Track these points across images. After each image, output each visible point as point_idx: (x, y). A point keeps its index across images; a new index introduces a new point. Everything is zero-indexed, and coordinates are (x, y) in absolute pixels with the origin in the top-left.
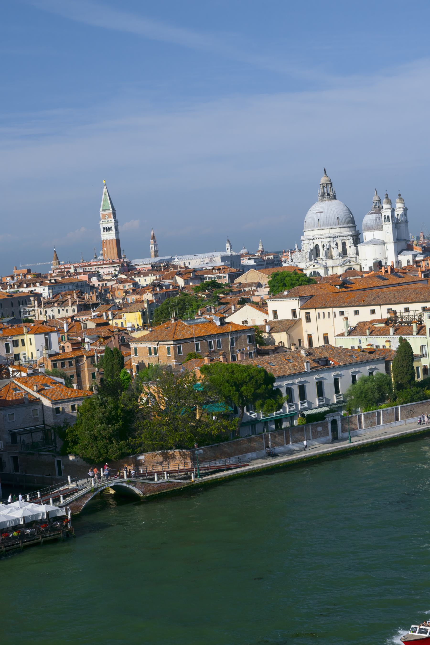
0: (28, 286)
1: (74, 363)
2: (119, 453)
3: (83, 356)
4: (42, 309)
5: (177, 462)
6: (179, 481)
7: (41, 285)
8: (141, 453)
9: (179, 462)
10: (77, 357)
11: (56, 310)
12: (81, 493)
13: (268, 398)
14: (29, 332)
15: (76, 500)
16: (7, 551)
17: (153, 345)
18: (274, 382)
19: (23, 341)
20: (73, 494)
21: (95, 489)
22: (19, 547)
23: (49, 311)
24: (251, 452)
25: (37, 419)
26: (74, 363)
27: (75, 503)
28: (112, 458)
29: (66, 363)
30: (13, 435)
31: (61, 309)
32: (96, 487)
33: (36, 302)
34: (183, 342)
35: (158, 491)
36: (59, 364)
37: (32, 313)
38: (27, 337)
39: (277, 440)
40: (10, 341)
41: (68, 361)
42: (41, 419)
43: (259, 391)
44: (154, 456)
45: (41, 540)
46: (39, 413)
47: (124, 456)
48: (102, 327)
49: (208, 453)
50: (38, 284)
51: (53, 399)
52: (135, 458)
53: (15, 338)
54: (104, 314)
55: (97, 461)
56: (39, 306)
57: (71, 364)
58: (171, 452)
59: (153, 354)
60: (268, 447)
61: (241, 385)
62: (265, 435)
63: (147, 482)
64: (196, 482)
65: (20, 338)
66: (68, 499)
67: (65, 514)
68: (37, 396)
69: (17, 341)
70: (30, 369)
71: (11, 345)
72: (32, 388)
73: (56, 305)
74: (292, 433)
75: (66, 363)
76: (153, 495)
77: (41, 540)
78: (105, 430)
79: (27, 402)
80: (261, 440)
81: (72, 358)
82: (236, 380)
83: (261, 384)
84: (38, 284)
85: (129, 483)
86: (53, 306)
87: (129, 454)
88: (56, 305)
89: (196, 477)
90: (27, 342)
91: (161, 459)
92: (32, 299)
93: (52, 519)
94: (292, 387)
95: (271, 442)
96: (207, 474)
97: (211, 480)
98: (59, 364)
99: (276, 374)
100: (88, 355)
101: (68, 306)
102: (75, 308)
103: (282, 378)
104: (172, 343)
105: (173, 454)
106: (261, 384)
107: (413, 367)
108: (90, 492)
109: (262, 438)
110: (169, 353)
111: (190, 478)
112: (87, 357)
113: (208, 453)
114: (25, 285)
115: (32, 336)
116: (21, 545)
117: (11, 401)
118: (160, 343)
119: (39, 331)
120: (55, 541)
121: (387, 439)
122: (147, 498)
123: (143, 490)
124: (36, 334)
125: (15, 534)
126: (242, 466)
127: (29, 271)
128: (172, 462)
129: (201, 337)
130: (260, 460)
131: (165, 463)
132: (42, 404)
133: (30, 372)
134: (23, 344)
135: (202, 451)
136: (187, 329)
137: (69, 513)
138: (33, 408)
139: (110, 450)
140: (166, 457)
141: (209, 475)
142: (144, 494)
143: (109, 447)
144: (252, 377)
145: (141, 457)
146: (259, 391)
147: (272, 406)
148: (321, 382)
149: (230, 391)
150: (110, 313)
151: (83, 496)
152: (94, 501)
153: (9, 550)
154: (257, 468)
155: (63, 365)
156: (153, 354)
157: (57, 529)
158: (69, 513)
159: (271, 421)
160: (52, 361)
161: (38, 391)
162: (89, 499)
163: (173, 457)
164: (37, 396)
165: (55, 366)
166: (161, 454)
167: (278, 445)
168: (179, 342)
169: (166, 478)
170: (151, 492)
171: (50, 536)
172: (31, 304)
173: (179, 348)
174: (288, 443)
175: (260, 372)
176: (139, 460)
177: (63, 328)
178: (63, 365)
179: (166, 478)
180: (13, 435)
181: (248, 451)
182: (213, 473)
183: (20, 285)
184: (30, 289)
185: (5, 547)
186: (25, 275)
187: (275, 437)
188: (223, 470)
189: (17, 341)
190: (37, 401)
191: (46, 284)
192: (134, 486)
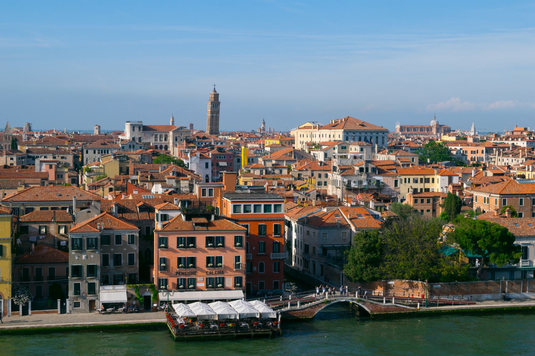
0: (512, 140)
1: (431, 201)
2: (371, 276)
3: (439, 197)
4: (501, 158)
5: (419, 291)
6: (405, 307)
7: (522, 140)
8: (391, 279)
9: (419, 291)
10: (435, 197)
11: (510, 159)
12: (317, 302)
13: (501, 253)
14: (438, 174)
15: (311, 307)
16: (222, 336)
17: (487, 196)
18: (514, 240)
19: (433, 179)
20: (311, 302)
21: (328, 302)
22: (233, 335)
23: (505, 159)
24: (487, 293)
25: (345, 240)
26: (431, 201)
27: (309, 309)
28: (365, 279)
29: (425, 200)
30: (325, 250)
31: (514, 159)
32: (329, 300)
33: (497, 152)
34: (508, 196)
35: (385, 311)
36: (419, 200)
37: (493, 160)
38: (437, 177)
39: (514, 287)
40: (398, 178)
41: (426, 199)
42: (348, 241)
43: (495, 245)
44: (402, 284)
45: (253, 334)
46: (347, 235)
47: (374, 279)
48: (497, 177)
49: (446, 288)
50: (520, 139)
51: (358, 227)
52: (386, 282)
53: (427, 177)
54: (527, 167)
55: (353, 279)
56: (499, 155)
57: (428, 201)
58: (415, 282)
59: (486, 203)
60: (504, 292)
61: (479, 239)
62: (502, 282)
63: (375, 303)
64: (421, 310)
65: (431, 177)
66: (303, 306)
67: (275, 317)
68: (349, 222)
69: (429, 179)
70: (353, 201)
71: (399, 182)
72: (347, 216)
73: (511, 156)
74: (529, 284)
75: (425, 200)
76: (379, 314)
77: (253, 334)
78: (362, 257)
79: (339, 226)
80: (498, 285)
81: (430, 197)
82: (475, 234)
83: (496, 240)
84: (520, 139)
85: (359, 301)
86: (509, 157)
87: (382, 279)
88: (511, 156)
89: (420, 306)
90: (436, 181)
91: (407, 286)
92: (494, 149)
93: (264, 320)
94: (528, 246)
95: (508, 288)
96: (435, 305)
97: (522, 307)
98: (419, 200)
99: (517, 234)
100: (443, 196)
101: (519, 157)
102: (524, 159)
103: (521, 238)
104: (499, 196)
105: (417, 284)
106: (496, 240)
107: (15, 263)
108: (323, 303)
109: (499, 284)
110: (496, 204)
111: (416, 306)
112: (442, 198)
113: (446, 288)
114: (510, 139)
115: (439, 177)
116: (235, 334)
117: (328, 223)
118: (492, 195)
119: (445, 174)
120: (265, 336)
121: (122, 325)
122: (374, 315)
123: (371, 309)
124: (441, 175)
125: (230, 325)
126: (469, 304)
127: (526, 129)
128: (416, 291)
129: (526, 194)
130: (493, 302)
131: (410, 291)
132: (351, 229)
133: (354, 204)
134: (433, 182)
135: (440, 286)
136: (517, 187)
137: (280, 317)
138: (343, 231)
139: (365, 273)
140: (412, 286)
141: (436, 306)
142: (372, 312)
143: (364, 270)
144: (490, 234)
145: (392, 283)
146: (495, 245)
147: (504, 259)
148: (527, 247)
149: (466, 242)
150: (531, 167)
151: (317, 305)
152: (324, 311)
153: (224, 336)
154: (481, 308)
155: (422, 201)
156: (486, 203)
157: (268, 327)
158: (280, 317)
159: (530, 271)
160: (414, 197)
161: (351, 219)
162: (322, 308)
163: (417, 286)
164: (349, 222)
165: (416, 201)
166: (408, 282)
167: (515, 292)
168: (505, 196)
169: (393, 302)
170: (378, 312)
171: (260, 331)
172: (493, 153)
173: (505, 201)
174: (524, 291)
175: (497, 230)
176: (390, 285)
177: (471, 174)
178: (422, 201)
179: (393, 302)
180: (325, 250)
181: (484, 292)
182: (440, 305)
183: (507, 138)
184: (513, 142)
185: (221, 333)
186: (522, 132)
187: (512, 284)
188: (451, 305)
189: (429, 179)
190: (347, 227)
191: (526, 140)
192: (364, 304)
